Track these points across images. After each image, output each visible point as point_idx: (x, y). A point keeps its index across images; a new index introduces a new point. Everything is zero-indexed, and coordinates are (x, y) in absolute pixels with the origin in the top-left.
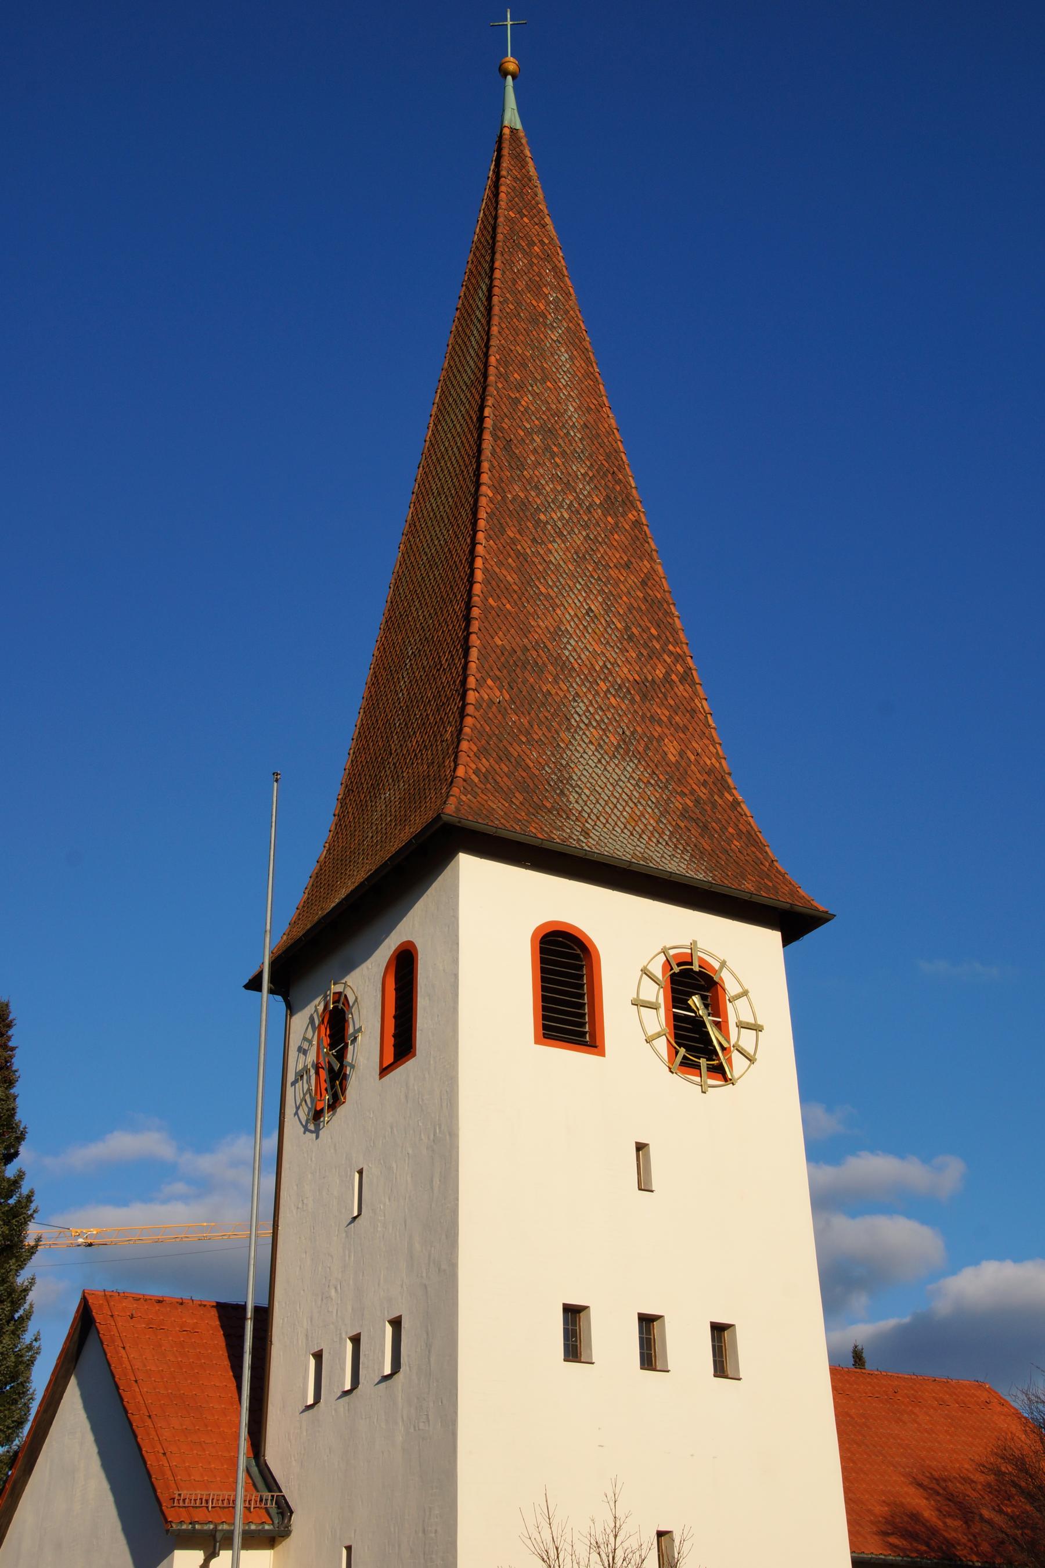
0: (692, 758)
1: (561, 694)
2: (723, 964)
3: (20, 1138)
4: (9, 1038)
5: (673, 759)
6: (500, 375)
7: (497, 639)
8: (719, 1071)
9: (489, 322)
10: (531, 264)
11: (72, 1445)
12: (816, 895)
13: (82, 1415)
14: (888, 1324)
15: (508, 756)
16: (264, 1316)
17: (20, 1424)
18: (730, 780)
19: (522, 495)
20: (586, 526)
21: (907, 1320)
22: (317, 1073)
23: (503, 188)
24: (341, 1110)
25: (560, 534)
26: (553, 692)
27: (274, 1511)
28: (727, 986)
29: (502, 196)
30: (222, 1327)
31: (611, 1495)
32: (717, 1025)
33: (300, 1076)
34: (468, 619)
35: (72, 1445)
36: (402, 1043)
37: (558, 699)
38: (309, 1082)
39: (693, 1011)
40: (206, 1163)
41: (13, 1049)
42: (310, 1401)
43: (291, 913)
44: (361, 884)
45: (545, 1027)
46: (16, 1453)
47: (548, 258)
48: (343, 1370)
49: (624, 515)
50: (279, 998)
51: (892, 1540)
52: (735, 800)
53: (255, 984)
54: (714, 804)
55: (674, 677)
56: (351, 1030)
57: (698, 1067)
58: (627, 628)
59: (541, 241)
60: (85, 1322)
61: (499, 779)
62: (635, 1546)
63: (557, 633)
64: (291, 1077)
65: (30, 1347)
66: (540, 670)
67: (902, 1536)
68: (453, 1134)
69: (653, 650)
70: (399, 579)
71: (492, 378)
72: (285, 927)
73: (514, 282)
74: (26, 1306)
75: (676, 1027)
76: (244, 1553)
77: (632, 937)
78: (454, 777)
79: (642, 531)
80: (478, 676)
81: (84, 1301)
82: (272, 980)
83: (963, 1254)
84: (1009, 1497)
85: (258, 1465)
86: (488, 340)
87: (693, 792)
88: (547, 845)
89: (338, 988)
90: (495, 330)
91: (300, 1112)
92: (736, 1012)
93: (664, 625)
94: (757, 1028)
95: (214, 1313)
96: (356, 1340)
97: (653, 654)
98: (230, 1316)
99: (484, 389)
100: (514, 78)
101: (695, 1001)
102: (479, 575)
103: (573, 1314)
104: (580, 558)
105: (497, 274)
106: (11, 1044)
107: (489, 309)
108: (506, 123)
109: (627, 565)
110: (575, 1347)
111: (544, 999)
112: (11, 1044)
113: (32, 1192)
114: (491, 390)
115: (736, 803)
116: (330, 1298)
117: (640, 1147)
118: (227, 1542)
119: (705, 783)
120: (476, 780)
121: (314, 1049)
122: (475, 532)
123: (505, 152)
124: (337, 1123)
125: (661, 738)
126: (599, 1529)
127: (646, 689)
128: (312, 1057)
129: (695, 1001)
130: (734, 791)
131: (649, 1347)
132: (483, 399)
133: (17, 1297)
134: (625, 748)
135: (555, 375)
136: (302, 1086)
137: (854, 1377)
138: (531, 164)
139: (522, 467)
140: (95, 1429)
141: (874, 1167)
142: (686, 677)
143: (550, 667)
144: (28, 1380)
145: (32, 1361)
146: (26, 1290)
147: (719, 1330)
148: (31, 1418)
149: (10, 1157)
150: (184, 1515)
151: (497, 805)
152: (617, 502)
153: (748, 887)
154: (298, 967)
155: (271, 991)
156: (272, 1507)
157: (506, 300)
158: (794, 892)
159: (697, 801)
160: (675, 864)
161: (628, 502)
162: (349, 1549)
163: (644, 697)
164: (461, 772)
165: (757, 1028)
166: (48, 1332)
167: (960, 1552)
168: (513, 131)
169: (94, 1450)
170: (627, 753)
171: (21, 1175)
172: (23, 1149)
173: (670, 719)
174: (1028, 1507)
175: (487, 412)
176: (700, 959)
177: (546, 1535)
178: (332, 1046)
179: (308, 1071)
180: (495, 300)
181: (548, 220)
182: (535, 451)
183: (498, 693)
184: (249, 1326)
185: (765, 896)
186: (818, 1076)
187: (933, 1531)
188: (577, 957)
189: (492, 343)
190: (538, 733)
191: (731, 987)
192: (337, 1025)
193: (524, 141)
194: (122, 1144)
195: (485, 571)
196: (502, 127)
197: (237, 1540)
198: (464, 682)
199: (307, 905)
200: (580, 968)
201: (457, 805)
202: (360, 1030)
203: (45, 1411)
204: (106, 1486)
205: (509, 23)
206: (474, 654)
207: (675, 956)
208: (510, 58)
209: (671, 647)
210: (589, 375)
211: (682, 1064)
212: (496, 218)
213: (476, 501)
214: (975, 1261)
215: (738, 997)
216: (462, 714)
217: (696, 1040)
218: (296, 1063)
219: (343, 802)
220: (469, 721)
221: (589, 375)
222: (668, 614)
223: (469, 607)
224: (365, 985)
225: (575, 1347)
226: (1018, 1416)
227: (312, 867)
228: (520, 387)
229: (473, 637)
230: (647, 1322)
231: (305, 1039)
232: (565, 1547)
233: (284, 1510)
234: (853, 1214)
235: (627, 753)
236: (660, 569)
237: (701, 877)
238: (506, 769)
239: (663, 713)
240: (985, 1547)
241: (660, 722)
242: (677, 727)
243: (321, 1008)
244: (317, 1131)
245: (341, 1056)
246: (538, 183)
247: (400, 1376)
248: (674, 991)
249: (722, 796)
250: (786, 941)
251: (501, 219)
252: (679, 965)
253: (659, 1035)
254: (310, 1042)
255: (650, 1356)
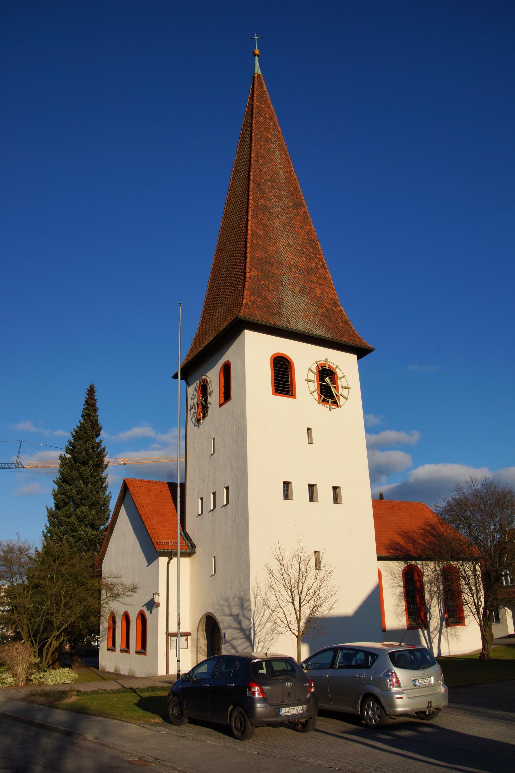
0: (325, 295)
1: (279, 273)
2: (337, 366)
3: (100, 429)
4: (95, 396)
5: (319, 295)
6: (255, 161)
7: (256, 254)
8: (335, 403)
9: (251, 142)
10: (266, 121)
11: (124, 527)
12: (368, 342)
13: (127, 517)
14: (394, 485)
15: (261, 295)
16: (183, 486)
17: (107, 519)
18: (339, 303)
19: (264, 203)
20: (287, 214)
21: (400, 484)
22: (198, 406)
23: (255, 95)
24: (206, 419)
25: (278, 216)
26: (276, 272)
27: (190, 546)
28: (338, 374)
29: (255, 97)
30: (170, 490)
31: (299, 540)
32: (335, 387)
33: (192, 407)
34: (246, 247)
35: (124, 527)
36: (227, 396)
37: (278, 275)
38: (195, 409)
39: (326, 383)
40: (165, 438)
41: (96, 400)
42: (200, 513)
43: (187, 352)
44: (211, 341)
45: (275, 389)
46: (107, 528)
47: (272, 119)
48: (210, 503)
49: (300, 209)
50: (184, 381)
51: (390, 551)
52: (341, 309)
53: (175, 377)
54: (333, 311)
55: (319, 266)
56: (209, 392)
57: (328, 402)
58: (302, 249)
59: (269, 113)
60: (125, 488)
61: (258, 303)
62: (307, 555)
63: (277, 252)
64: (189, 408)
65: (108, 496)
66: (271, 265)
67: (393, 550)
68: (245, 426)
69: (311, 257)
70: (221, 234)
71: (252, 162)
72: (185, 357)
73: (260, 128)
74: (106, 483)
75: (321, 388)
76: (181, 558)
77: (305, 358)
78: (242, 303)
79: (306, 215)
80: (250, 267)
81: (124, 481)
82: (181, 375)
83: (418, 462)
84: (428, 536)
85: (184, 532)
86: (251, 148)
87: (326, 307)
88: (275, 326)
89: (204, 377)
90: (253, 145)
91: (193, 419)
92: (341, 383)
93: (315, 248)
94: (348, 388)
95: (167, 485)
96: (214, 494)
97: (311, 259)
98: (172, 486)
99: (250, 166)
100: (258, 56)
101: (327, 379)
102: (249, 232)
103: (287, 485)
104: (285, 225)
105: (254, 125)
106: (95, 398)
107: (251, 138)
108: (256, 72)
109: (302, 227)
110: (287, 495)
111: (275, 379)
112: (95, 398)
113: (105, 447)
114: (252, 166)
115: (341, 311)
116: (205, 480)
117: (309, 429)
118: (176, 555)
119: (330, 304)
120: (250, 304)
121: (197, 398)
122: (248, 216)
123: (256, 82)
124: (205, 423)
125: (314, 288)
126: (296, 551)
127: (309, 271)
128: (196, 401)
129: (327, 379)
130: (340, 307)
131: (312, 495)
132: (250, 169)
133: (103, 480)
134: (302, 292)
135: (275, 160)
136: (193, 411)
137: (380, 503)
138: (265, 86)
139: (264, 193)
140: (131, 521)
141: (390, 435)
142: (323, 266)
143: (275, 264)
144: (108, 506)
145: (109, 500)
146: (105, 478)
147: (335, 489)
148: (111, 517)
149: (98, 435)
150: (161, 547)
151: (258, 313)
152: (298, 205)
153: (345, 340)
154: (190, 371)
155: (181, 379)
156: (189, 545)
157: (257, 134)
158: (361, 341)
159: (327, 310)
160: (320, 332)
161: (302, 205)
162: (214, 557)
163: (308, 274)
164: (244, 301)
165: (348, 388)
166: (114, 492)
167: (411, 553)
168: (258, 75)
169: (131, 527)
170: (303, 293)
171: (101, 442)
172: (102, 432)
173: (317, 281)
174: (433, 539)
175: (251, 174)
176: (329, 365)
177: (279, 553)
178: (203, 397)
179: (194, 405)
180: (253, 134)
181: (271, 106)
182: (268, 187)
183: (257, 273)
184: (179, 489)
185: (351, 343)
186: (369, 405)
187: (403, 548)
188: (286, 365)
189: (252, 149)
190: (271, 287)
191: (339, 374)
192: (204, 390)
193: (262, 78)
194: (137, 431)
195: (252, 230)
196: (254, 74)
197: (179, 554)
198: (245, 270)
199: (192, 349)
200: (287, 369)
201: (243, 313)
202: (212, 391)
203: (115, 515)
204: (136, 538)
205: (256, 38)
206: (248, 260)
207: (320, 364)
208: (257, 50)
209: (317, 256)
210: (287, 160)
211: (323, 401)
212: (253, 105)
213: (248, 205)
214: (423, 464)
215: (342, 378)
216: (245, 281)
217: (327, 394)
218: (190, 403)
219: (204, 313)
220: (247, 283)
221: (287, 160)
222: (317, 244)
223: (246, 243)
224: (213, 376)
225: (287, 495)
226: (432, 512)
227: (194, 336)
228: (262, 165)
229: (248, 254)
230: (311, 487)
231: (193, 395)
232: (285, 556)
233: (193, 546)
234: (382, 451)
235: (303, 293)
236: (313, 228)
237: (329, 336)
238: (260, 300)
239: (315, 279)
240: (419, 551)
241: (314, 282)
242: (320, 284)
243: (198, 384)
244: (198, 426)
245: (206, 400)
246: (267, 93)
247: (229, 505)
248: (320, 376)
249: (336, 308)
250: (358, 358)
251: (255, 106)
252: (321, 367)
253: (315, 391)
254: (195, 396)
255: (312, 498)
